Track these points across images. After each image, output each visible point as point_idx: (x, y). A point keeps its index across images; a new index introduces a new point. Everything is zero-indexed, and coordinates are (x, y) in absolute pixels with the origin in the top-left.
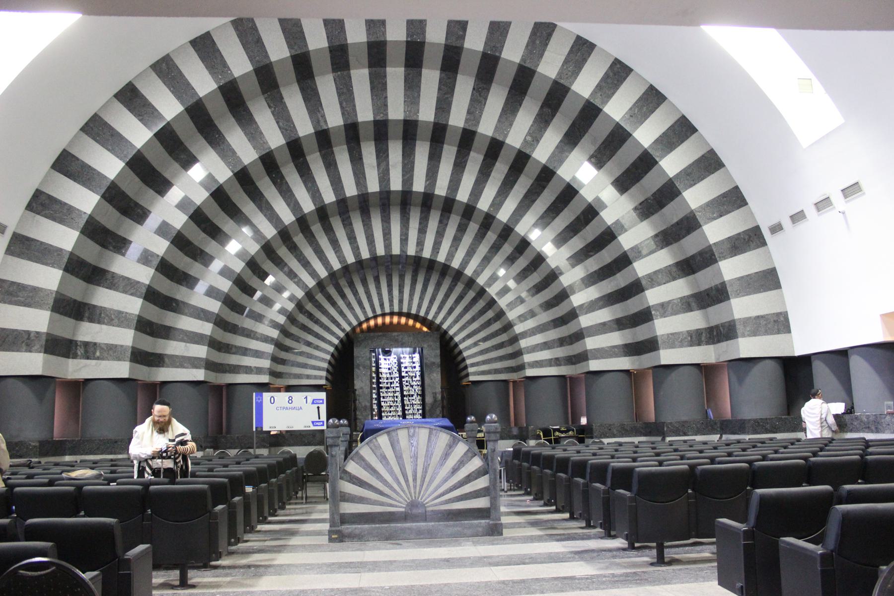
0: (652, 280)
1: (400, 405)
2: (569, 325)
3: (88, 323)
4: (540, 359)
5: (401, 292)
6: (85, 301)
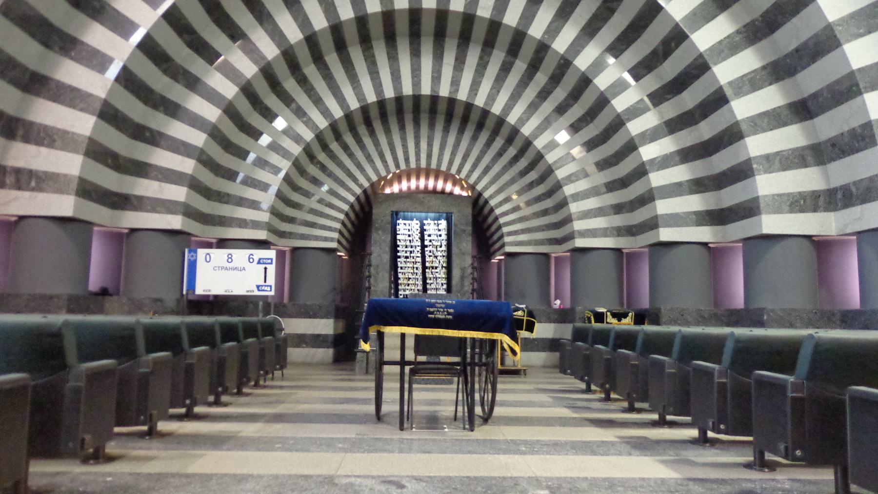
0: (756, 125)
1: (420, 277)
2: (629, 188)
4: (593, 226)
5: (430, 145)
6: (19, 115)
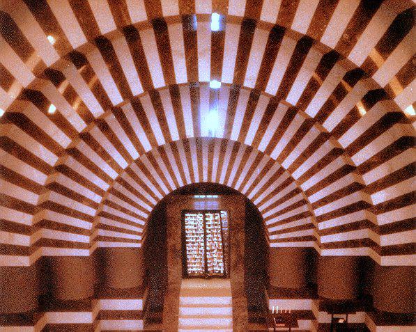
3: (107, 71)
